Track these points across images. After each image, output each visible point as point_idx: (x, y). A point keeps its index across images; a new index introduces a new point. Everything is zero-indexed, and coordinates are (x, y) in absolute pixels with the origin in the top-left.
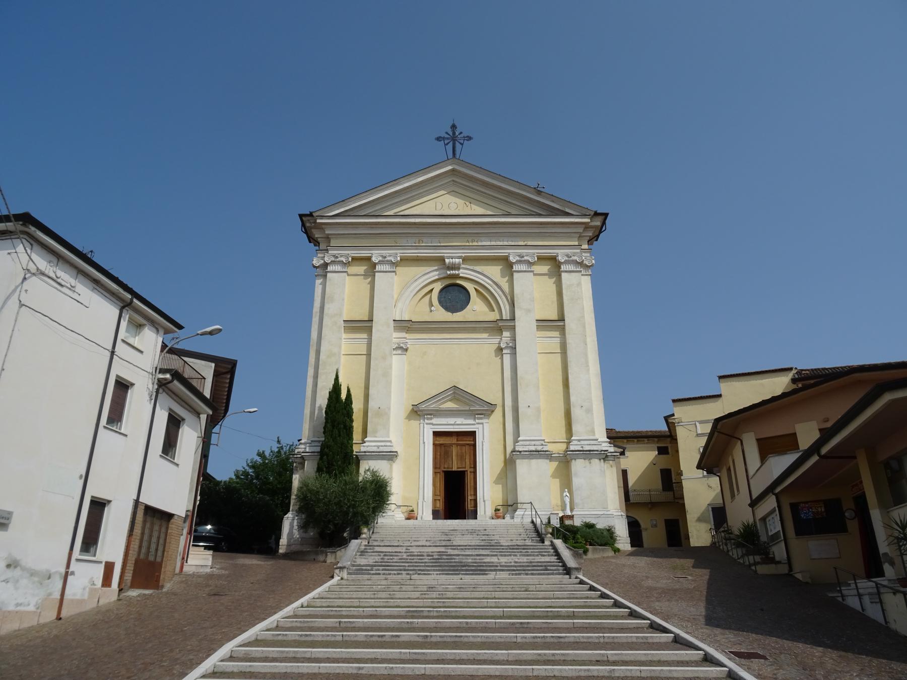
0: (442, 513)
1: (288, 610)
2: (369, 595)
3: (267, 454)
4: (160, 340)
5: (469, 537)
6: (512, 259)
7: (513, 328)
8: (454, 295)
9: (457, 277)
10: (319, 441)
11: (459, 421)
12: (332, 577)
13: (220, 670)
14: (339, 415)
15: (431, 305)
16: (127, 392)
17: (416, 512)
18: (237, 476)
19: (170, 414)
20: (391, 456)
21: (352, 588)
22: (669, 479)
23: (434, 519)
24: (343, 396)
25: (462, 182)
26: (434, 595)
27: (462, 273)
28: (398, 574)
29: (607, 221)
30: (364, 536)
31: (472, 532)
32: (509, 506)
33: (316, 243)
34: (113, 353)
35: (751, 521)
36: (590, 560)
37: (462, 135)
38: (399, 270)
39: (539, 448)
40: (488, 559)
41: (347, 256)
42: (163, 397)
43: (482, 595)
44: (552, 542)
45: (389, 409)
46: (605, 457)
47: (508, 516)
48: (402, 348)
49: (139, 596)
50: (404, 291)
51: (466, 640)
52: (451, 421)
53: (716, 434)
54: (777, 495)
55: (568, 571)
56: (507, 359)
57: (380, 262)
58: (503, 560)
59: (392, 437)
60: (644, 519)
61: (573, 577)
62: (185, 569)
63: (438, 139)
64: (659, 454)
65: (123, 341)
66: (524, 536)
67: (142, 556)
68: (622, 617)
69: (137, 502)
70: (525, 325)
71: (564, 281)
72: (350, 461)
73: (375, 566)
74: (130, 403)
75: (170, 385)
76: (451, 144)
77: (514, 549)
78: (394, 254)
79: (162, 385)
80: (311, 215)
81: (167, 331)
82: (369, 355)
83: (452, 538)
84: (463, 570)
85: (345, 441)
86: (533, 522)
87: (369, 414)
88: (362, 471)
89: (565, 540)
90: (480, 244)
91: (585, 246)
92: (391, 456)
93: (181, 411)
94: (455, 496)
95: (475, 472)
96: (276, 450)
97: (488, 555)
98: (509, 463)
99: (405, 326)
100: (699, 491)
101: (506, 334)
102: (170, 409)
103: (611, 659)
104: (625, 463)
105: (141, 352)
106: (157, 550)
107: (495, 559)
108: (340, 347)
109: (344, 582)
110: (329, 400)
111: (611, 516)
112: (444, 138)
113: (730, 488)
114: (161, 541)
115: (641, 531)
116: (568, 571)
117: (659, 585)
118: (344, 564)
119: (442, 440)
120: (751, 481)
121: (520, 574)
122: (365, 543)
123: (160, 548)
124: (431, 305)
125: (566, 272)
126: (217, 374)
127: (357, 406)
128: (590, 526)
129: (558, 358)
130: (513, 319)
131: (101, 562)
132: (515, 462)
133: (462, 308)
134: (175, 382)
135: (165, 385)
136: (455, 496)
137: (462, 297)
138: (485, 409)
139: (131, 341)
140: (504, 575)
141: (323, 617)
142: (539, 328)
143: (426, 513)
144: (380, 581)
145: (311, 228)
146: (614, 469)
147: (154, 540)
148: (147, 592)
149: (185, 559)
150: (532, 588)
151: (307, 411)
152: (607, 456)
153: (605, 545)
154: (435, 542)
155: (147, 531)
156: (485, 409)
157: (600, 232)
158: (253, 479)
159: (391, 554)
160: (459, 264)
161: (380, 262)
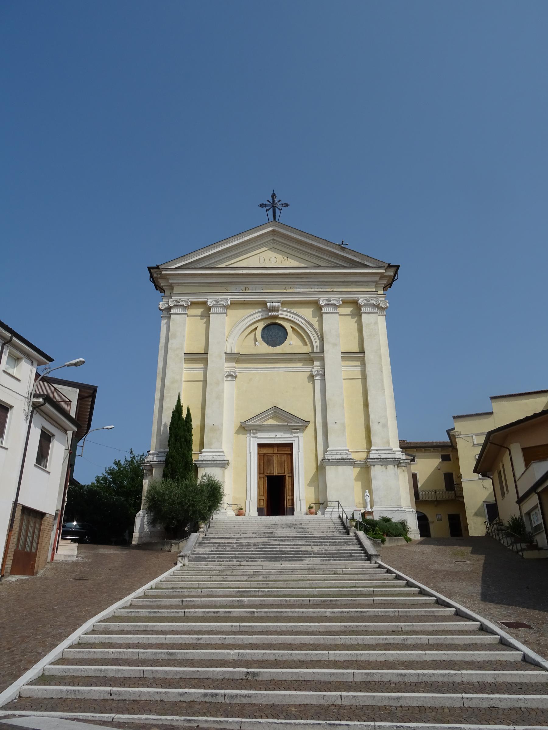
0: (265, 511)
1: (140, 591)
2: (206, 578)
3: (122, 463)
4: (34, 370)
6: (322, 303)
7: (322, 359)
8: (274, 332)
9: (277, 317)
10: (164, 452)
11: (279, 434)
12: (176, 564)
13: (85, 641)
14: (180, 430)
15: (256, 340)
16: (7, 413)
17: (244, 509)
18: (98, 481)
20: (223, 464)
21: (192, 573)
22: (451, 481)
23: (258, 515)
24: (184, 415)
25: (280, 241)
26: (260, 578)
27: (281, 314)
28: (230, 561)
30: (202, 530)
31: (290, 526)
32: (321, 504)
33: (162, 290)
35: (518, 515)
36: (391, 548)
37: (280, 203)
38: (229, 312)
39: (345, 457)
40: (303, 548)
41: (187, 301)
42: (37, 417)
43: (299, 577)
44: (355, 533)
45: (222, 425)
46: (398, 463)
47: (319, 513)
48: (232, 375)
49: (17, 580)
50: (233, 329)
51: (285, 615)
53: (489, 444)
55: (369, 557)
56: (318, 384)
57: (214, 306)
58: (316, 549)
60: (431, 514)
61: (373, 562)
63: (261, 206)
64: (443, 460)
66: (333, 529)
68: (413, 595)
69: (16, 503)
70: (332, 356)
71: (363, 321)
73: (211, 554)
74: (10, 421)
75: (42, 407)
76: (271, 211)
77: (324, 539)
79: (36, 407)
80: (157, 267)
81: (40, 363)
82: (205, 381)
83: (274, 530)
84: (283, 557)
85: (186, 452)
86: (340, 517)
87: (206, 430)
88: (199, 476)
89: (367, 532)
90: (295, 290)
91: (381, 292)
92: (223, 464)
94: (276, 496)
96: (130, 459)
97: (303, 545)
99: (234, 357)
100: (476, 491)
101: (317, 364)
102: (43, 427)
103: (404, 629)
105: (19, 380)
106: (32, 543)
107: (309, 548)
108: (182, 375)
109: (185, 568)
110: (172, 418)
111: (404, 512)
112: (266, 205)
113: (501, 488)
116: (369, 557)
117: (443, 568)
118: (186, 553)
119: (265, 451)
120: (518, 482)
121: (329, 560)
124: (256, 340)
125: (365, 313)
126: (81, 398)
127: (195, 423)
128: (387, 520)
132: (325, 468)
133: (281, 343)
134: (47, 405)
135: (38, 407)
136: (276, 496)
138: (300, 425)
140: (316, 561)
141: (168, 597)
142: (343, 358)
143: (252, 510)
144: (214, 566)
145: (157, 277)
147: (30, 534)
148: (24, 577)
149: (55, 550)
150: (340, 571)
152: (400, 463)
153: (399, 535)
154: (260, 534)
156: (300, 425)
157: (393, 281)
158: (111, 484)
159: (224, 545)
160: (278, 307)
161: (214, 306)
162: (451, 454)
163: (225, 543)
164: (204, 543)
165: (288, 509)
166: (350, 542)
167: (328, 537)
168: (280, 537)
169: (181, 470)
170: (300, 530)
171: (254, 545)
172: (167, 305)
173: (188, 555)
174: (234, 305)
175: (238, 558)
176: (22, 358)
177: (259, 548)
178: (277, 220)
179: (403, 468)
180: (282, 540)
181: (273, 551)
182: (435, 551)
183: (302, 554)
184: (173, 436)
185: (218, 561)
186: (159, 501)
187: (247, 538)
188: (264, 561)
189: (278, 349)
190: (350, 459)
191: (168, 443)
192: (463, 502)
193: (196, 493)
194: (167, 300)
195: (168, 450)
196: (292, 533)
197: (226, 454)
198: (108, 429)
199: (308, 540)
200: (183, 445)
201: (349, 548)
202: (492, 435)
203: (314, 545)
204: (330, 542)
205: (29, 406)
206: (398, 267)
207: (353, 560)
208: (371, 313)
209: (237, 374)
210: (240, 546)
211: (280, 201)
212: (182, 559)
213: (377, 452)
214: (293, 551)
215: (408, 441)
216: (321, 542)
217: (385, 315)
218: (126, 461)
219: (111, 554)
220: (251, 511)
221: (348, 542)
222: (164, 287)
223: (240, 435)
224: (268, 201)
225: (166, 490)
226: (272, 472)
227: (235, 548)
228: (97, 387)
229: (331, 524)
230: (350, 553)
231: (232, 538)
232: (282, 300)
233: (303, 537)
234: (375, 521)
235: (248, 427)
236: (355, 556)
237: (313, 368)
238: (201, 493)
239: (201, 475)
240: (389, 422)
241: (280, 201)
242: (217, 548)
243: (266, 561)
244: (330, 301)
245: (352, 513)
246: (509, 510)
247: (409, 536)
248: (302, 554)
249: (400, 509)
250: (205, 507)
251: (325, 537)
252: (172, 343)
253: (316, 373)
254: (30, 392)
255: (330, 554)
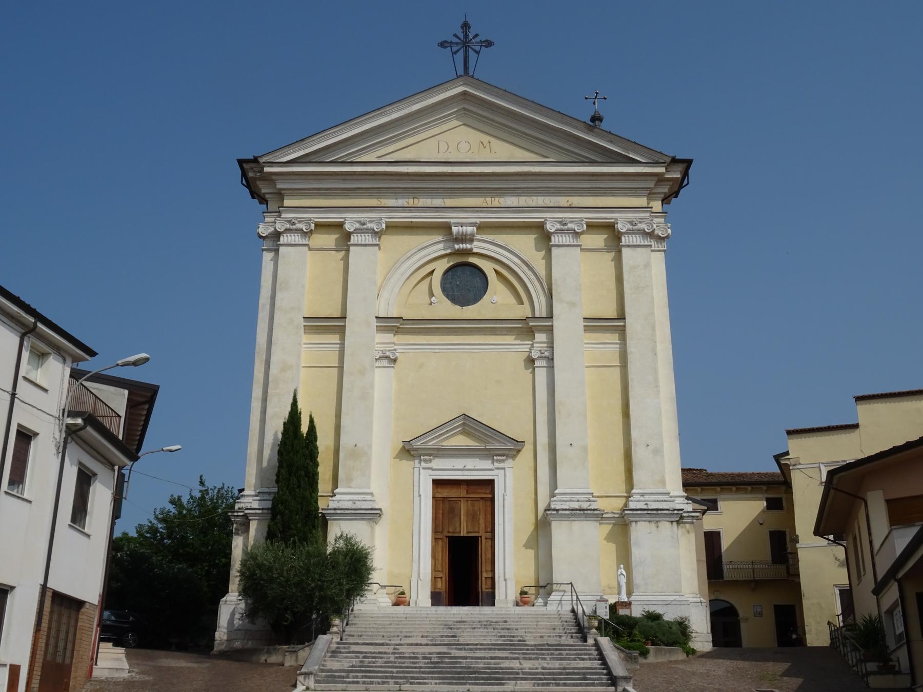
0: (445, 596)
3: (185, 500)
4: (68, 371)
5: (482, 631)
6: (550, 227)
7: (550, 330)
8: (464, 280)
9: (470, 253)
10: (269, 493)
11: (471, 463)
12: (295, 686)
14: (297, 454)
15: (431, 294)
16: (29, 444)
17: (407, 594)
19: (79, 469)
20: (373, 515)
22: (782, 545)
23: (433, 605)
24: (304, 429)
25: (474, 111)
27: (476, 247)
28: (384, 683)
29: (690, 171)
30: (335, 629)
31: (487, 625)
33: (263, 200)
34: (13, 395)
35: (875, 613)
36: (649, 665)
37: (478, 39)
38: (387, 240)
39: (585, 505)
40: (506, 664)
41: (308, 222)
42: (72, 448)
44: (596, 640)
45: (370, 447)
46: (679, 518)
48: (388, 358)
50: (392, 273)
52: (459, 463)
53: (832, 491)
54: (899, 582)
56: (541, 375)
57: (357, 231)
58: (527, 665)
59: (374, 488)
60: (743, 604)
62: (96, 673)
63: (443, 44)
64: (769, 507)
65: (25, 378)
66: (559, 631)
67: (49, 657)
69: (44, 587)
70: (568, 324)
72: (316, 522)
73: (352, 671)
74: (34, 458)
75: (81, 433)
76: (461, 54)
77: (543, 649)
78: (377, 220)
79: (71, 433)
80: (255, 160)
81: (76, 359)
82: (341, 368)
83: (458, 633)
84: (471, 679)
85: (307, 494)
86: (573, 611)
88: (331, 538)
89: (616, 636)
91: (657, 206)
92: (373, 515)
93: (92, 464)
94: (464, 572)
95: (493, 539)
96: (198, 495)
97: (506, 658)
98: (542, 526)
99: (392, 325)
100: (822, 568)
101: (541, 337)
102: (80, 463)
104: (710, 522)
105: (46, 390)
106: (65, 649)
107: (515, 664)
111: (686, 603)
112: (451, 44)
113: (853, 563)
114: (70, 638)
115: (739, 622)
116: (613, 680)
118: (311, 669)
119: (445, 493)
120: (877, 559)
121: (548, 684)
122: (337, 639)
123: (69, 646)
124: (431, 294)
125: (629, 246)
126: (132, 405)
127: (324, 443)
128: (654, 617)
129: (617, 372)
130: (550, 317)
131: (5, 665)
132: (550, 525)
134: (89, 428)
135: (75, 432)
136: (464, 572)
137: (478, 281)
139: (31, 377)
142: (587, 329)
143: (421, 595)
145: (255, 180)
146: (692, 536)
149: (94, 660)
151: (253, 449)
152: (682, 517)
153: (673, 644)
154: (434, 638)
155: (54, 625)
157: (681, 187)
158: (163, 539)
159: (374, 656)
160: (472, 235)
161: (357, 231)
162: (784, 496)
163: (374, 653)
164: (340, 652)
165: (484, 594)
166: (585, 654)
167: (548, 645)
168: (468, 645)
169: (299, 525)
170: (503, 633)
171: (424, 658)
172: (272, 229)
173: (314, 672)
174: (393, 228)
175: (396, 678)
176: (49, 354)
177: (431, 663)
178: (471, 74)
179: (688, 526)
180: (471, 649)
181: (455, 668)
182: (728, 672)
183: (503, 673)
184: (285, 465)
185: (364, 683)
186: (263, 580)
187: (412, 645)
188: (440, 684)
189: (470, 312)
190: (594, 510)
191: (275, 478)
192: (799, 583)
193: (326, 568)
194: (272, 219)
195: (276, 490)
196: (490, 637)
197: (377, 497)
198: (171, 451)
199: (515, 649)
200: (302, 483)
201: (582, 664)
202: (836, 477)
203: (525, 659)
204: (552, 654)
205: (60, 431)
206: (689, 163)
207: (587, 685)
208: (639, 246)
209: (397, 355)
210: (400, 658)
211: (477, 35)
212: (305, 678)
213: (642, 498)
214: (489, 668)
215: (709, 471)
216: (537, 654)
217: (664, 251)
218: (192, 497)
219: (182, 668)
220: (420, 597)
221: (581, 654)
222: (267, 196)
223: (404, 462)
224: (455, 36)
225: (275, 561)
226: (458, 530)
227: (391, 662)
228: (158, 387)
229: (557, 623)
230: (584, 674)
231: (387, 644)
232: (478, 221)
233: (507, 645)
234: (634, 619)
235: (416, 449)
236: (590, 679)
237: (532, 345)
238: (333, 567)
239: (334, 537)
240: (666, 445)
241: (477, 35)
242: (361, 662)
243: (444, 683)
244: (566, 224)
245: (594, 603)
246: (867, 606)
247: (692, 645)
248: (503, 673)
249: (678, 598)
250: (341, 590)
251: (543, 645)
252: (282, 298)
253: (539, 354)
254: (62, 407)
255: (550, 674)
